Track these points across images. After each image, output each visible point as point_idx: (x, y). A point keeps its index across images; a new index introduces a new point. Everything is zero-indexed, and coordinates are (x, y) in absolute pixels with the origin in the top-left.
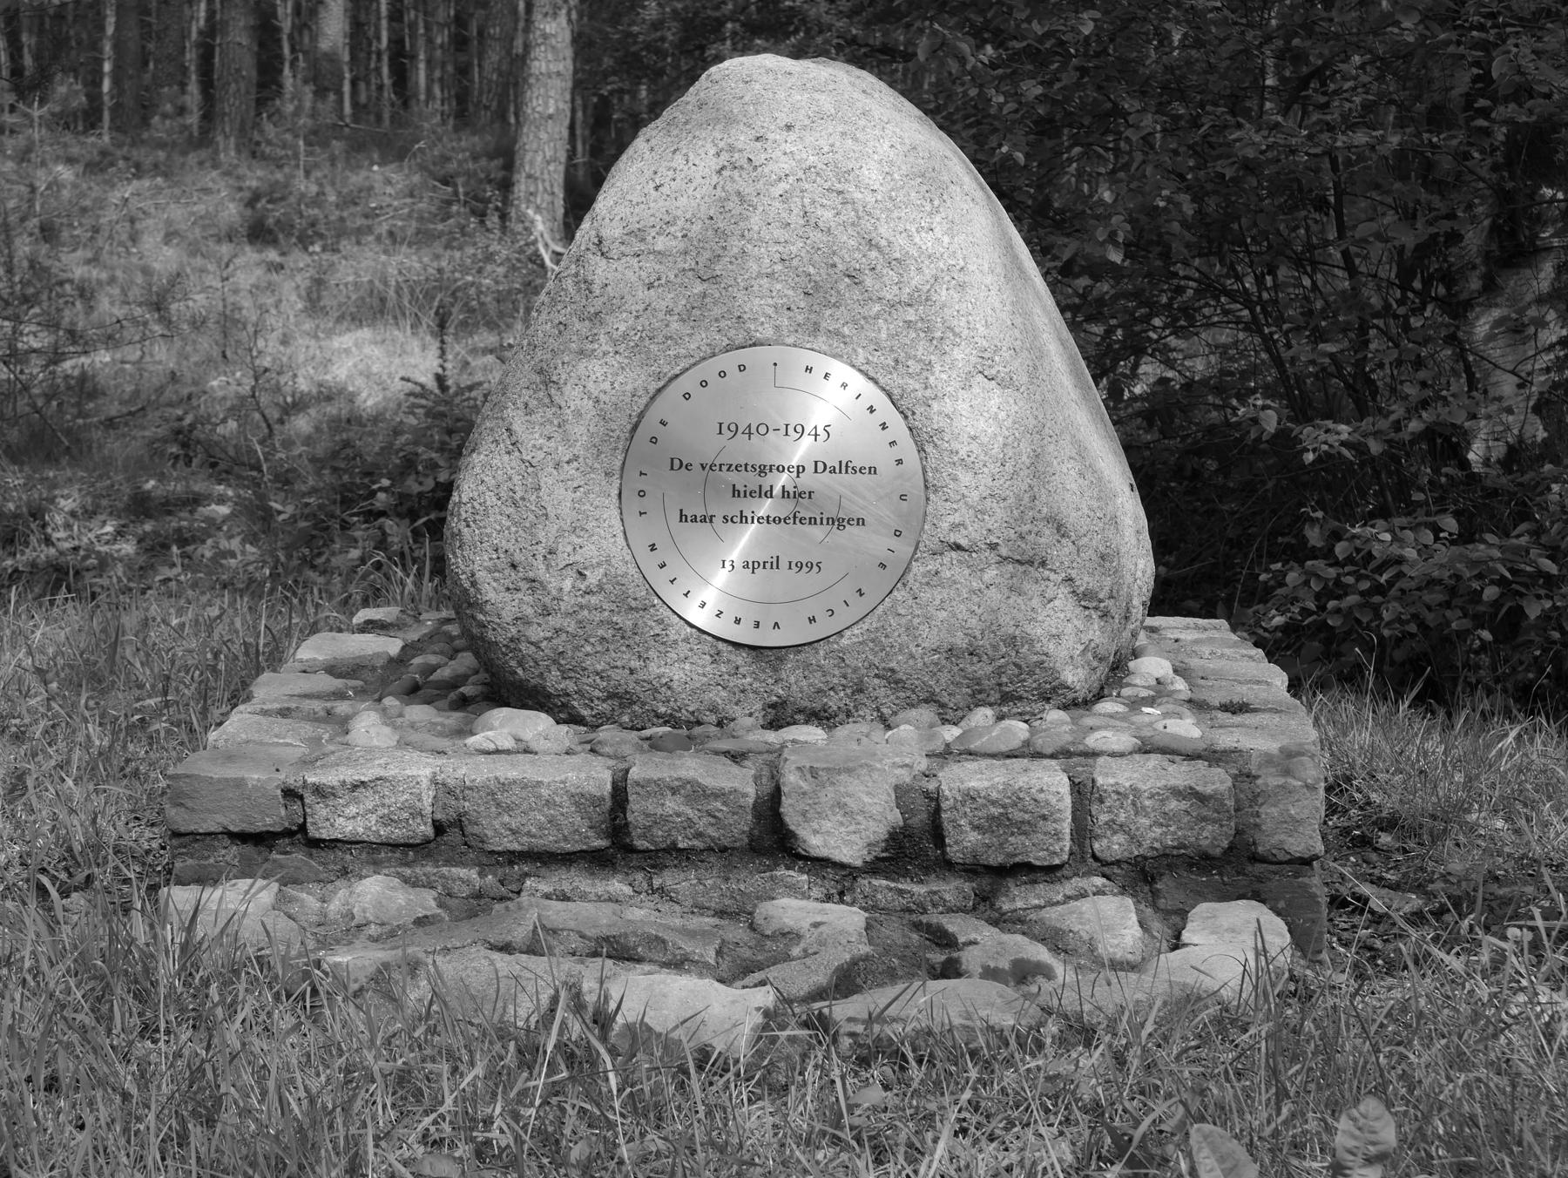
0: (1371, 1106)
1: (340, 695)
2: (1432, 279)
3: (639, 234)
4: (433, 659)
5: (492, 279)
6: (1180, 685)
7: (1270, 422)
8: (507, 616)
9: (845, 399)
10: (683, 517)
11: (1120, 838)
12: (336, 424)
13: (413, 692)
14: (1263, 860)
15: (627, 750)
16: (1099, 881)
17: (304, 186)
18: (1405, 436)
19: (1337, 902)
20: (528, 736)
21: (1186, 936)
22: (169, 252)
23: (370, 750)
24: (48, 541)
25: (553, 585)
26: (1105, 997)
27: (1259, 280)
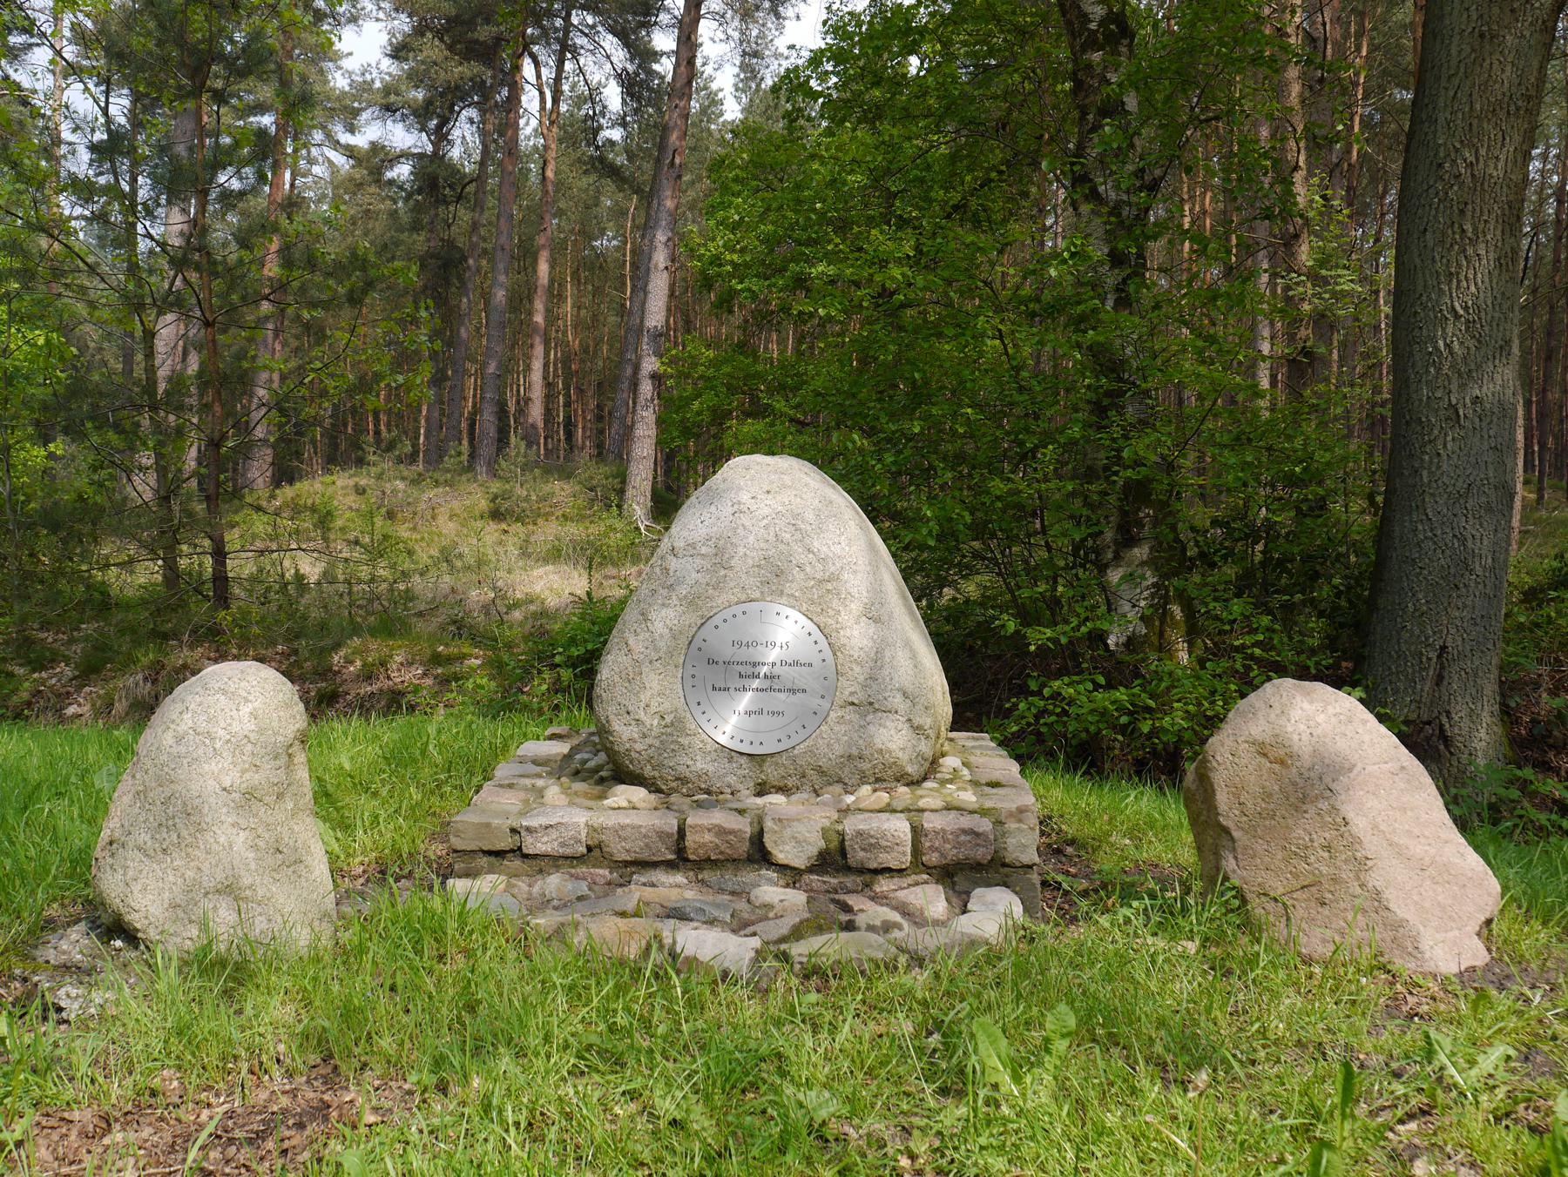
0: (1062, 1007)
1: (539, 776)
2: (1091, 558)
3: (693, 546)
4: (586, 756)
5: (615, 539)
6: (965, 772)
7: (1011, 626)
8: (625, 738)
9: (796, 629)
10: (714, 688)
11: (936, 855)
12: (535, 616)
13: (576, 774)
14: (1008, 866)
15: (685, 807)
16: (925, 877)
17: (521, 492)
18: (1078, 634)
19: (1044, 884)
20: (635, 799)
21: (969, 906)
22: (451, 525)
23: (555, 807)
24: (389, 678)
25: (648, 724)
26: (927, 940)
27: (1003, 553)
